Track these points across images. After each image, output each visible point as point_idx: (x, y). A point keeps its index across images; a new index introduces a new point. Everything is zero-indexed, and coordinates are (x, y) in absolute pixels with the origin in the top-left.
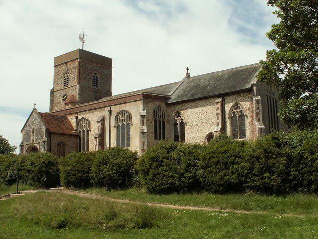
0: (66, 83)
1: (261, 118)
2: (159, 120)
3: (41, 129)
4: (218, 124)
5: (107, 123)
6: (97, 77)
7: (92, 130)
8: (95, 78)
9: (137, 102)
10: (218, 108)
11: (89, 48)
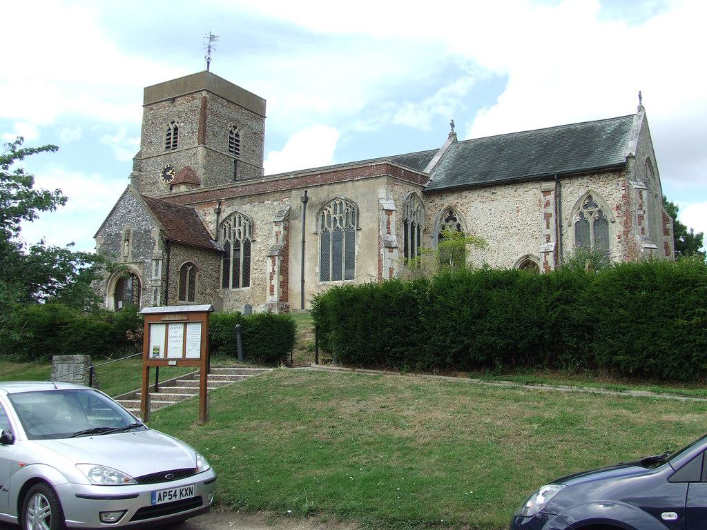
0: (172, 141)
1: (647, 228)
2: (412, 224)
3: (148, 232)
4: (548, 238)
5: (297, 224)
6: (237, 135)
7: (259, 240)
8: (233, 136)
9: (374, 180)
10: (548, 204)
11: (215, 69)
